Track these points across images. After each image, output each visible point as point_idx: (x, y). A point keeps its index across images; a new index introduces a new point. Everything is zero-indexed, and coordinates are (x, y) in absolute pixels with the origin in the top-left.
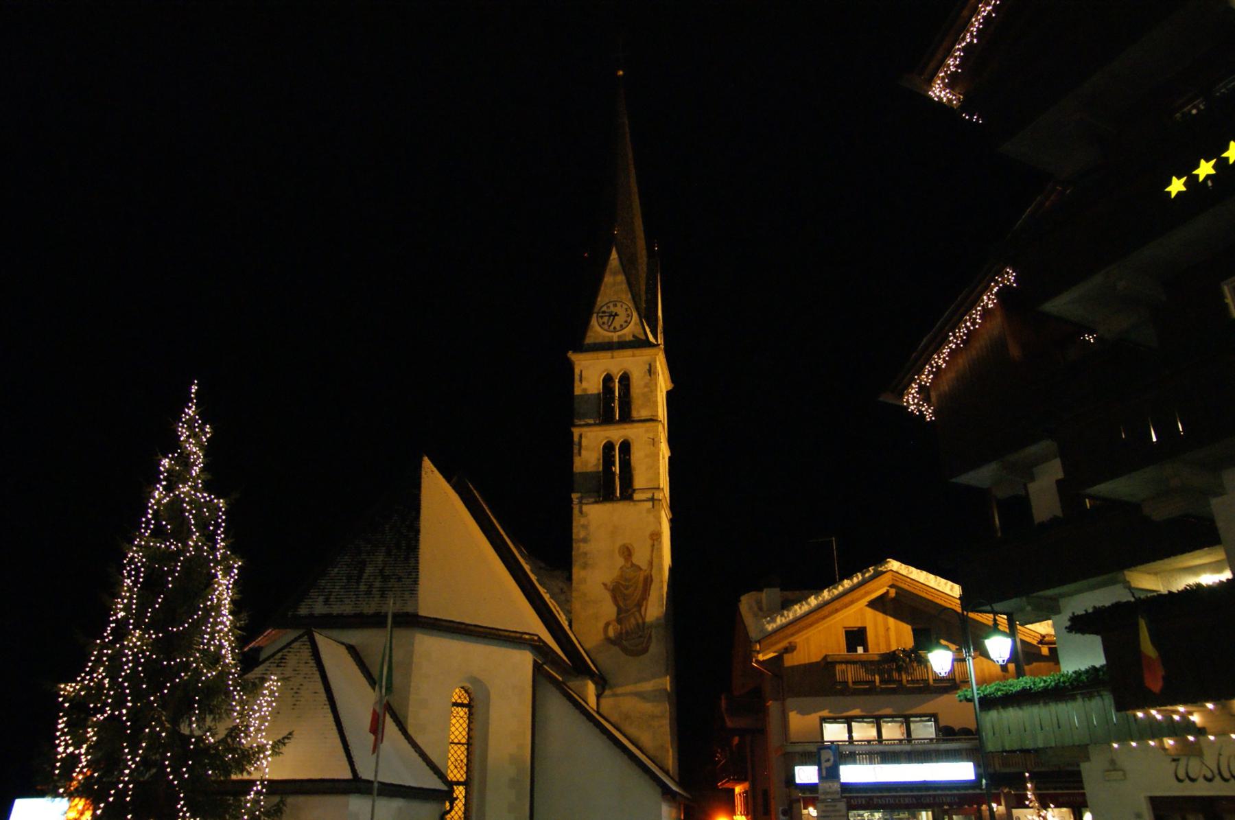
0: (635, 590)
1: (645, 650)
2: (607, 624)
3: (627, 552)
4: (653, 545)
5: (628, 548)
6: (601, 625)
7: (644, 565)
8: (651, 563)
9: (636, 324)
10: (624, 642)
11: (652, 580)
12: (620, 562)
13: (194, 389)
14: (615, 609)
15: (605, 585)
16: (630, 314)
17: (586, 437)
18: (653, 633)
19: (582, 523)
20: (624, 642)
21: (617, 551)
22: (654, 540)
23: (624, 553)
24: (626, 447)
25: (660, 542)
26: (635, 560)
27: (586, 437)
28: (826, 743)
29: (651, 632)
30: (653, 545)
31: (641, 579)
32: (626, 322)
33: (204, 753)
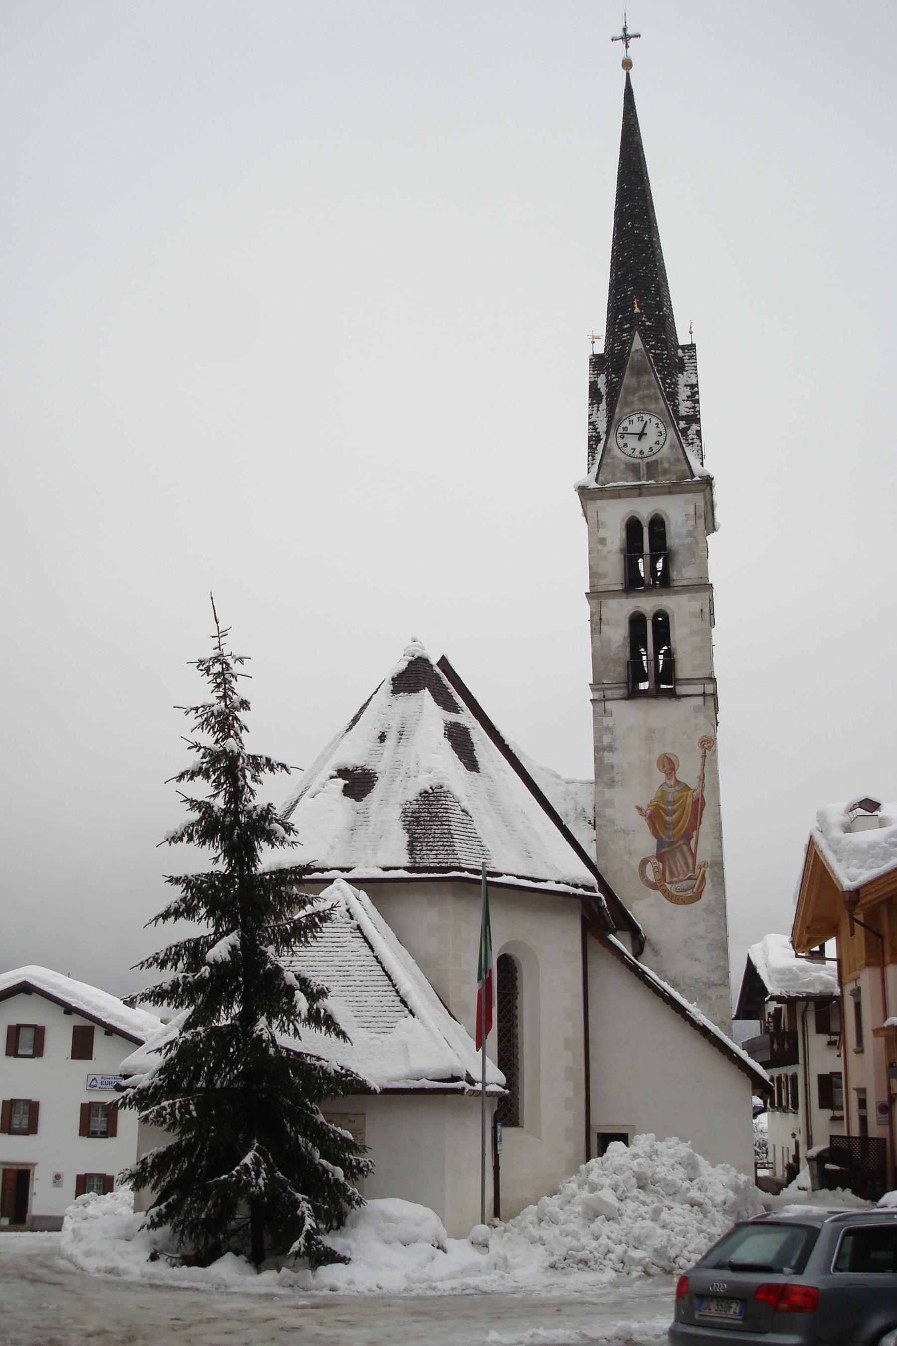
0: (682, 814)
1: (698, 896)
2: (644, 863)
3: (669, 765)
4: (704, 756)
5: (670, 761)
6: (636, 863)
7: (693, 783)
8: (702, 779)
9: (672, 446)
10: (668, 886)
11: (703, 804)
12: (660, 777)
13: (290, 1072)
14: (654, 841)
15: (639, 809)
16: (624, 449)
17: (607, 607)
18: (707, 875)
19: (605, 724)
20: (668, 886)
21: (655, 764)
22: (705, 749)
23: (664, 766)
24: (662, 623)
25: (715, 751)
26: (680, 775)
27: (607, 607)
28: (804, 954)
29: (704, 872)
30: (704, 756)
31: (689, 801)
32: (657, 443)
33: (172, 987)
